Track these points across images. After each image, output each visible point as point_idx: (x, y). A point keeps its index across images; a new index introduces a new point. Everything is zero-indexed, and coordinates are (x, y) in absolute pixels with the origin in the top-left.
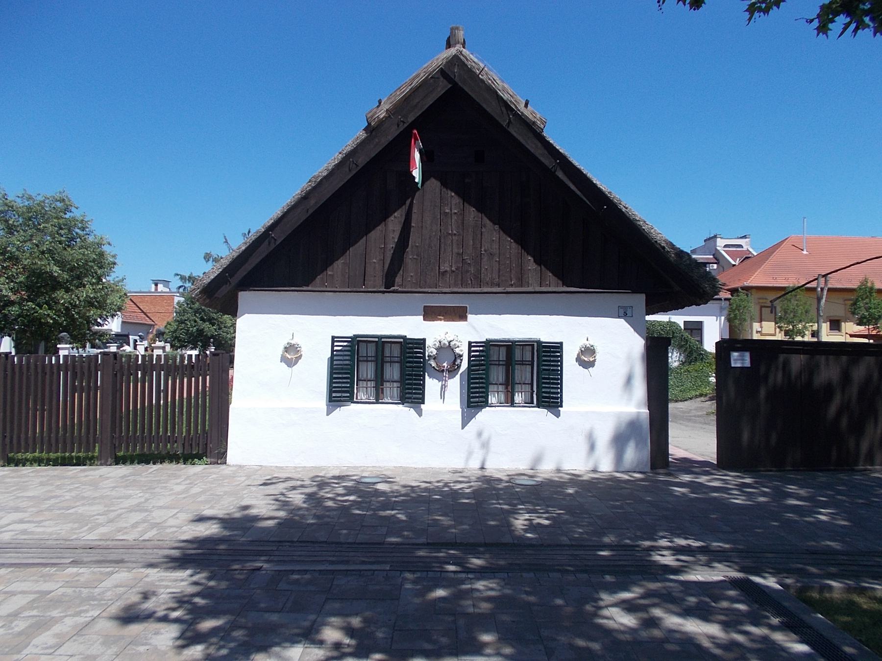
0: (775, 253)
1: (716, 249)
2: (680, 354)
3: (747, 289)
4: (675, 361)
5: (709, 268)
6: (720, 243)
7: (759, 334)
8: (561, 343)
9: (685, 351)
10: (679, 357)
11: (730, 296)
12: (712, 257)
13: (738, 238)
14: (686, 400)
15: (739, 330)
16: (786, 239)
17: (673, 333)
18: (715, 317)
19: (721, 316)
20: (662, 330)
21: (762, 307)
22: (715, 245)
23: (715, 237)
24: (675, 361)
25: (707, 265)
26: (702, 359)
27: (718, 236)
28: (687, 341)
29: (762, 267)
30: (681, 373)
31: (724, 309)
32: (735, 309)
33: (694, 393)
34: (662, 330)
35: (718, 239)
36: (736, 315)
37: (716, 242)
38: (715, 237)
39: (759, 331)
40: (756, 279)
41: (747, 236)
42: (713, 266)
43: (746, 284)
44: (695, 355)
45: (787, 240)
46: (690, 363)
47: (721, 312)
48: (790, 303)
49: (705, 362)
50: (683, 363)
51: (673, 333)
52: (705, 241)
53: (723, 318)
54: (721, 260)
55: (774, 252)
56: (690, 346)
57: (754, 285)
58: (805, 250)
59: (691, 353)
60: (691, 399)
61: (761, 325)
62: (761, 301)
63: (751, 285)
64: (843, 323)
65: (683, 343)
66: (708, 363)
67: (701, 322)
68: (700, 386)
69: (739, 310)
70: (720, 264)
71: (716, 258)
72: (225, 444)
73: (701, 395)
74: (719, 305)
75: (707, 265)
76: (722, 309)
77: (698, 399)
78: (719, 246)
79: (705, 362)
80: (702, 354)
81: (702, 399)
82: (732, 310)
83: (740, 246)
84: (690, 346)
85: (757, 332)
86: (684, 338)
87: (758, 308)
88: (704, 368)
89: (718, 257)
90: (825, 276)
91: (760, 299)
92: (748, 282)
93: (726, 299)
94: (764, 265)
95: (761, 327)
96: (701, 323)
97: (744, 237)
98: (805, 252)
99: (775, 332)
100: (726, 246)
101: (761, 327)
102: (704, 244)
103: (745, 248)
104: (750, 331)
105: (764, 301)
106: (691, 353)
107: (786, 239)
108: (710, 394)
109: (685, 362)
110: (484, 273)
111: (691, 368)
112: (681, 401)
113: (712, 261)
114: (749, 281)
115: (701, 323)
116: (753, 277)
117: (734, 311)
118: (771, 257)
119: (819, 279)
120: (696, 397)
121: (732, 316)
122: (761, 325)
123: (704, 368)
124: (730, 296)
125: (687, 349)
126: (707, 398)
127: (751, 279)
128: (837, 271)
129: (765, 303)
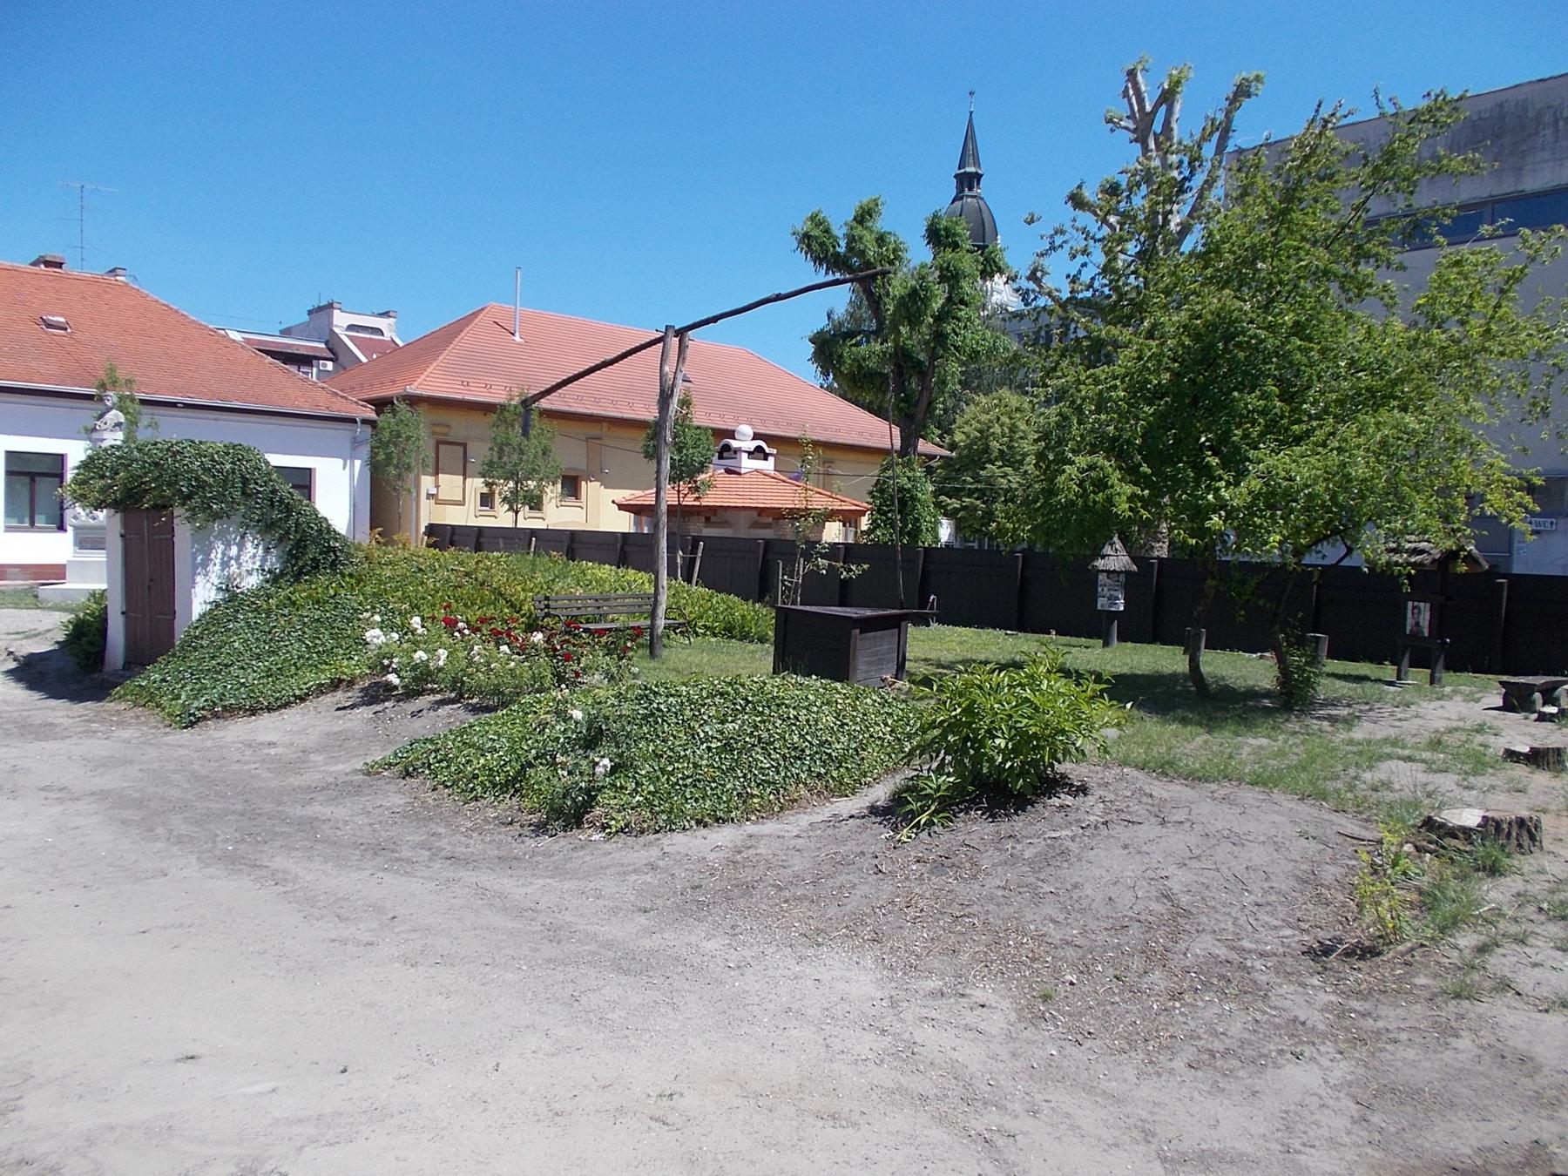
0: (463, 334)
1: (332, 332)
2: (267, 550)
3: (414, 401)
4: (249, 573)
5: (318, 367)
6: (340, 321)
7: (433, 501)
8: (6, 531)
9: (281, 540)
10: (264, 560)
11: (373, 416)
12: (323, 346)
13: (373, 315)
14: (286, 705)
15: (395, 489)
16: (483, 309)
17: (245, 481)
18: (340, 461)
19: (352, 458)
20: (207, 470)
21: (439, 443)
22: (331, 323)
23: (330, 306)
24: (249, 573)
25: (315, 362)
26: (333, 565)
27: (335, 305)
28: (288, 509)
29: (441, 358)
30: (269, 612)
31: (362, 443)
32: (389, 442)
33: (311, 679)
34: (207, 470)
35: (335, 311)
36: (389, 456)
37: (331, 316)
38: (330, 306)
39: (433, 495)
40: (430, 382)
41: (391, 314)
42: (325, 365)
43: (412, 389)
44: (312, 552)
45: (484, 312)
46: (297, 577)
47: (354, 449)
48: (513, 430)
49: (343, 575)
50: (275, 579)
51: (245, 481)
52: (310, 313)
53: (358, 463)
54: (341, 358)
55: (461, 331)
56: (297, 524)
57: (425, 393)
58: (517, 334)
59: (300, 546)
60: (302, 699)
61: (437, 481)
62: (437, 429)
63: (419, 392)
64: (583, 483)
65: (275, 515)
66: (351, 576)
67: (310, 469)
68: (330, 652)
69: (395, 445)
70: (339, 361)
71: (330, 350)
72: (849, 396)
73: (335, 685)
74: (348, 434)
75: (315, 362)
76: (356, 442)
77: (328, 699)
78: (337, 326)
79: (343, 575)
80: (334, 550)
81: (340, 696)
82: (379, 445)
83: (379, 331)
84: (297, 524)
85: (429, 496)
86: (281, 501)
87: (431, 443)
88: (343, 592)
89: (336, 348)
90: (681, 333)
91: (434, 425)
92: (413, 387)
93: (365, 421)
94: (444, 355)
95: (437, 486)
96: (308, 473)
97: (386, 314)
98: (517, 338)
99: (464, 498)
100: (351, 327)
101: (437, 486)
102: (307, 318)
103: (387, 337)
104: (414, 495)
105: (444, 430)
106: (300, 546)
107: (483, 309)
108: (362, 677)
109: (282, 574)
110: (679, 732)
111: (301, 593)
112: (269, 709)
113: (325, 355)
114: (416, 383)
115: (308, 473)
116: (423, 377)
117: (386, 445)
118: (457, 340)
119: (668, 340)
120: (321, 690)
121: (381, 457)
122: (437, 481)
123: (343, 592)
124: (373, 416)
125: (288, 533)
126: (355, 694)
127: (419, 380)
128: (715, 319)
129: (447, 435)
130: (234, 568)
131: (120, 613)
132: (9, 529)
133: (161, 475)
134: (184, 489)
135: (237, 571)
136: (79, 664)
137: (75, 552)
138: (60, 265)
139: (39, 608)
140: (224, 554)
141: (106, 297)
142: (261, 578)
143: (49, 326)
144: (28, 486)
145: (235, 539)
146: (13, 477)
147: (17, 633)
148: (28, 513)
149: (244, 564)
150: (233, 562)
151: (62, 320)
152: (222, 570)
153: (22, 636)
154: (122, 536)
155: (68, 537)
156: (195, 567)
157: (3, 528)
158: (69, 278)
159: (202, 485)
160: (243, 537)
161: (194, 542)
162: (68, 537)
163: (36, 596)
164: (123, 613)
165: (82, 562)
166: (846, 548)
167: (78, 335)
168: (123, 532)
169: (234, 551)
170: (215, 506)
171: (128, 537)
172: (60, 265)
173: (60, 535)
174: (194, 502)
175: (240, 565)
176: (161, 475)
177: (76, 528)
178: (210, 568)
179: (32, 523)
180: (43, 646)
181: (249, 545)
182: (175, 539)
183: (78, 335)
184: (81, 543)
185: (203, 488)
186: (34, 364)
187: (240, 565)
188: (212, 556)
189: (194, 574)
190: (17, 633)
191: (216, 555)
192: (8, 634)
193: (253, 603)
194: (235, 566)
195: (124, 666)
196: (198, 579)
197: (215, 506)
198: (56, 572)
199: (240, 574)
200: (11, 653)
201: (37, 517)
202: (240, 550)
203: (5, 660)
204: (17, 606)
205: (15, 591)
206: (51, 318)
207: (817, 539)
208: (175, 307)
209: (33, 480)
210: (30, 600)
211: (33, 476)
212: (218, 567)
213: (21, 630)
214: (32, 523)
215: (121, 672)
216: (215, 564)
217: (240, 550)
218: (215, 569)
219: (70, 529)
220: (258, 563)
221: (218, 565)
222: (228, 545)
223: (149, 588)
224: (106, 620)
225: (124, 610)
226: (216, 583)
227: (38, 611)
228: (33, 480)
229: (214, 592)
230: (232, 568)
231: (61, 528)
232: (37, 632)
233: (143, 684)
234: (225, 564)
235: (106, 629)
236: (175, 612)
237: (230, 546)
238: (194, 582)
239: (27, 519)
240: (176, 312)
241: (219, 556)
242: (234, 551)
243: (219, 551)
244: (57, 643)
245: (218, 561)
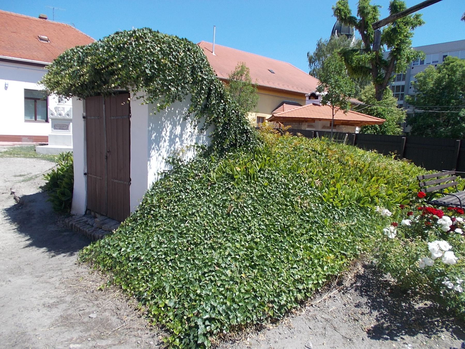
2: (201, 130)
4: (188, 148)
20: (165, 55)
24: (188, 148)
46: (222, 152)
98: (214, 54)
109: (211, 149)
130: (178, 145)
131: (83, 174)
132: (26, 121)
133: (126, 57)
134: (148, 71)
135: (180, 146)
136: (54, 208)
137: (52, 131)
138: (46, 19)
139: (35, 157)
140: (171, 132)
141: (63, 30)
142: (196, 153)
143: (41, 39)
144: (34, 103)
145: (179, 120)
146: (29, 100)
147: (21, 176)
148: (34, 115)
149: (185, 141)
150: (177, 139)
151: (46, 37)
152: (170, 146)
153: (22, 178)
154: (84, 117)
155: (49, 125)
156: (150, 143)
157: (24, 121)
158: (49, 23)
159: (162, 69)
160: (185, 119)
161: (150, 120)
162: (49, 125)
163: (35, 150)
164: (85, 174)
165: (56, 135)
166: (406, 138)
167: (52, 44)
168: (85, 114)
169: (178, 130)
170: (173, 89)
171: (89, 118)
172: (46, 19)
173: (46, 124)
174: (155, 85)
175: (182, 142)
176: (126, 57)
177: (52, 119)
178: (161, 144)
179: (36, 119)
180: (32, 189)
181: (189, 125)
182: (131, 119)
183: (52, 44)
184: (54, 126)
185: (164, 71)
186: (35, 53)
187: (182, 142)
188: (163, 133)
189: (149, 149)
190: (21, 176)
191: (166, 134)
192: (15, 176)
193: (197, 175)
194: (179, 143)
195: (86, 212)
196: (153, 153)
197: (173, 89)
198: (43, 140)
199: (182, 150)
200: (13, 193)
201: (38, 117)
202: (182, 130)
203: (9, 198)
204: (25, 156)
205: (27, 148)
206: (42, 37)
207: (354, 132)
208: (89, 36)
209: (35, 101)
210: (32, 153)
211: (35, 100)
212: (167, 143)
213: (23, 174)
214: (36, 119)
215: (85, 219)
216: (165, 141)
217: (182, 130)
218: (165, 145)
219: (50, 120)
220: (194, 141)
221: (167, 141)
222: (174, 126)
223: (107, 158)
224: (73, 172)
225: (86, 172)
226: (165, 157)
227: (35, 159)
228: (35, 101)
229: (163, 164)
230: (177, 145)
231: (47, 121)
232: (29, 176)
233: (114, 255)
234: (172, 141)
235: (72, 184)
236: (130, 180)
237: (176, 126)
238: (149, 156)
239: (34, 117)
240: (89, 38)
241: (168, 134)
242: (178, 130)
243: (168, 130)
244: (41, 187)
245: (167, 138)
